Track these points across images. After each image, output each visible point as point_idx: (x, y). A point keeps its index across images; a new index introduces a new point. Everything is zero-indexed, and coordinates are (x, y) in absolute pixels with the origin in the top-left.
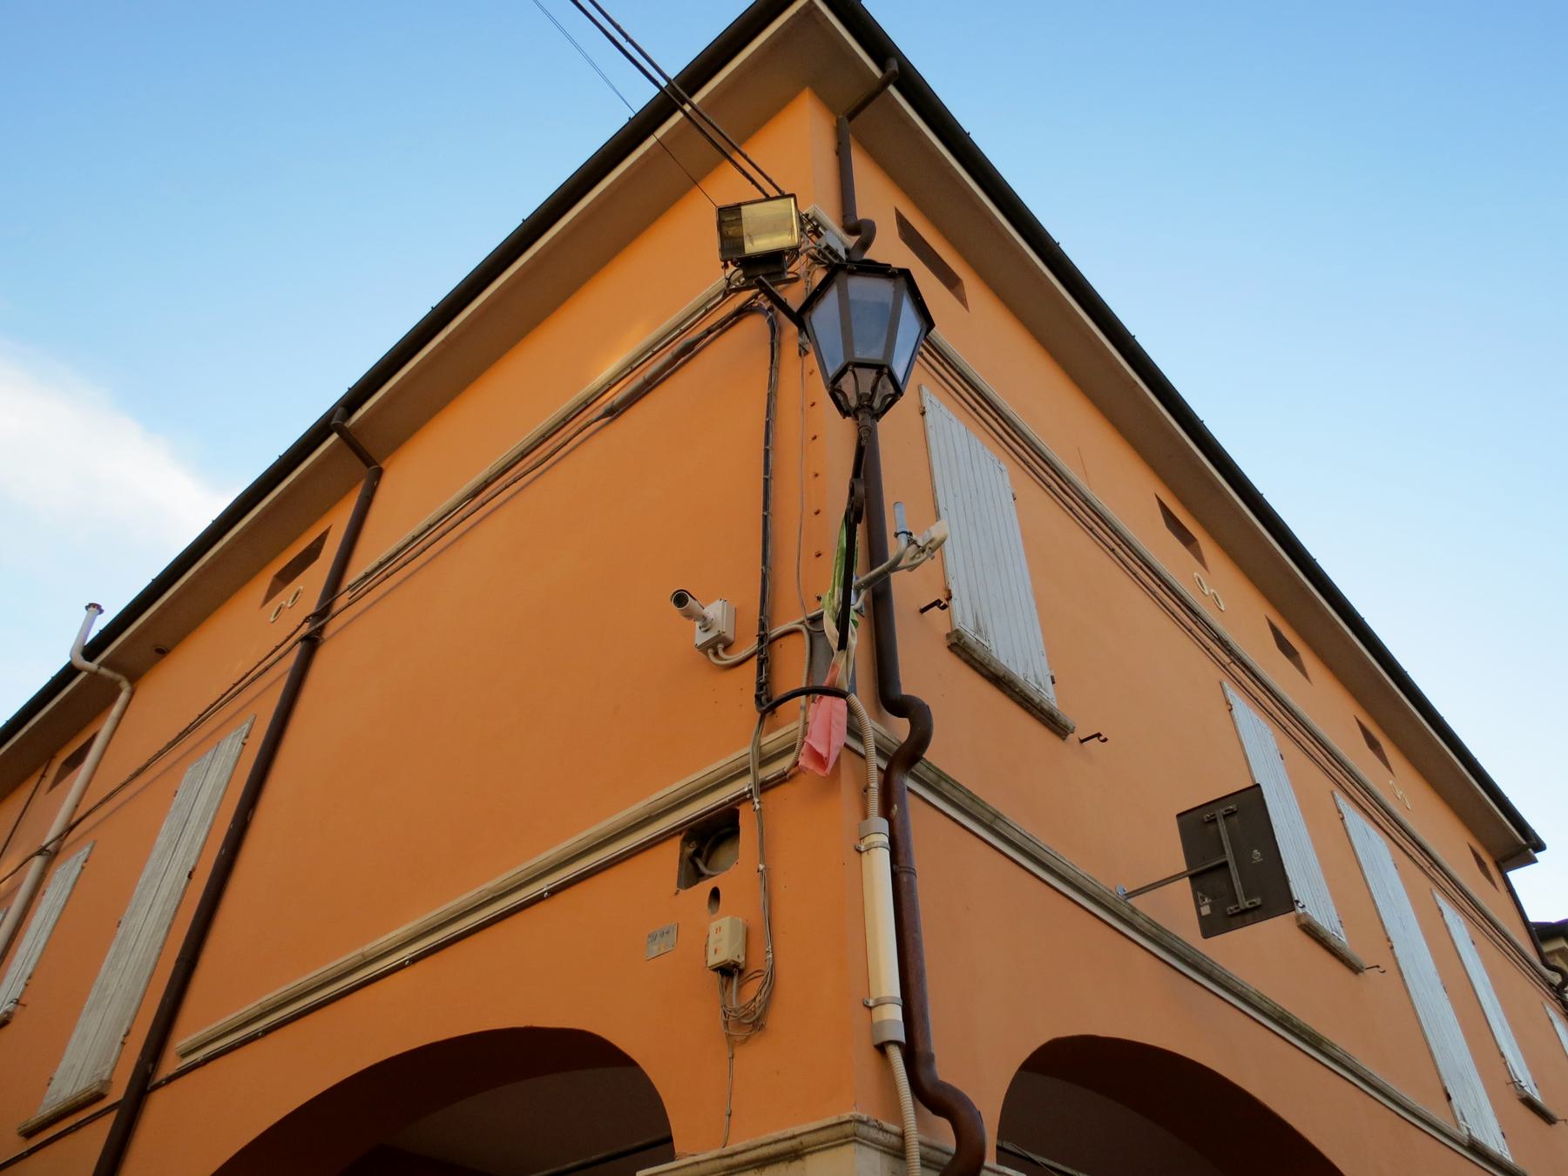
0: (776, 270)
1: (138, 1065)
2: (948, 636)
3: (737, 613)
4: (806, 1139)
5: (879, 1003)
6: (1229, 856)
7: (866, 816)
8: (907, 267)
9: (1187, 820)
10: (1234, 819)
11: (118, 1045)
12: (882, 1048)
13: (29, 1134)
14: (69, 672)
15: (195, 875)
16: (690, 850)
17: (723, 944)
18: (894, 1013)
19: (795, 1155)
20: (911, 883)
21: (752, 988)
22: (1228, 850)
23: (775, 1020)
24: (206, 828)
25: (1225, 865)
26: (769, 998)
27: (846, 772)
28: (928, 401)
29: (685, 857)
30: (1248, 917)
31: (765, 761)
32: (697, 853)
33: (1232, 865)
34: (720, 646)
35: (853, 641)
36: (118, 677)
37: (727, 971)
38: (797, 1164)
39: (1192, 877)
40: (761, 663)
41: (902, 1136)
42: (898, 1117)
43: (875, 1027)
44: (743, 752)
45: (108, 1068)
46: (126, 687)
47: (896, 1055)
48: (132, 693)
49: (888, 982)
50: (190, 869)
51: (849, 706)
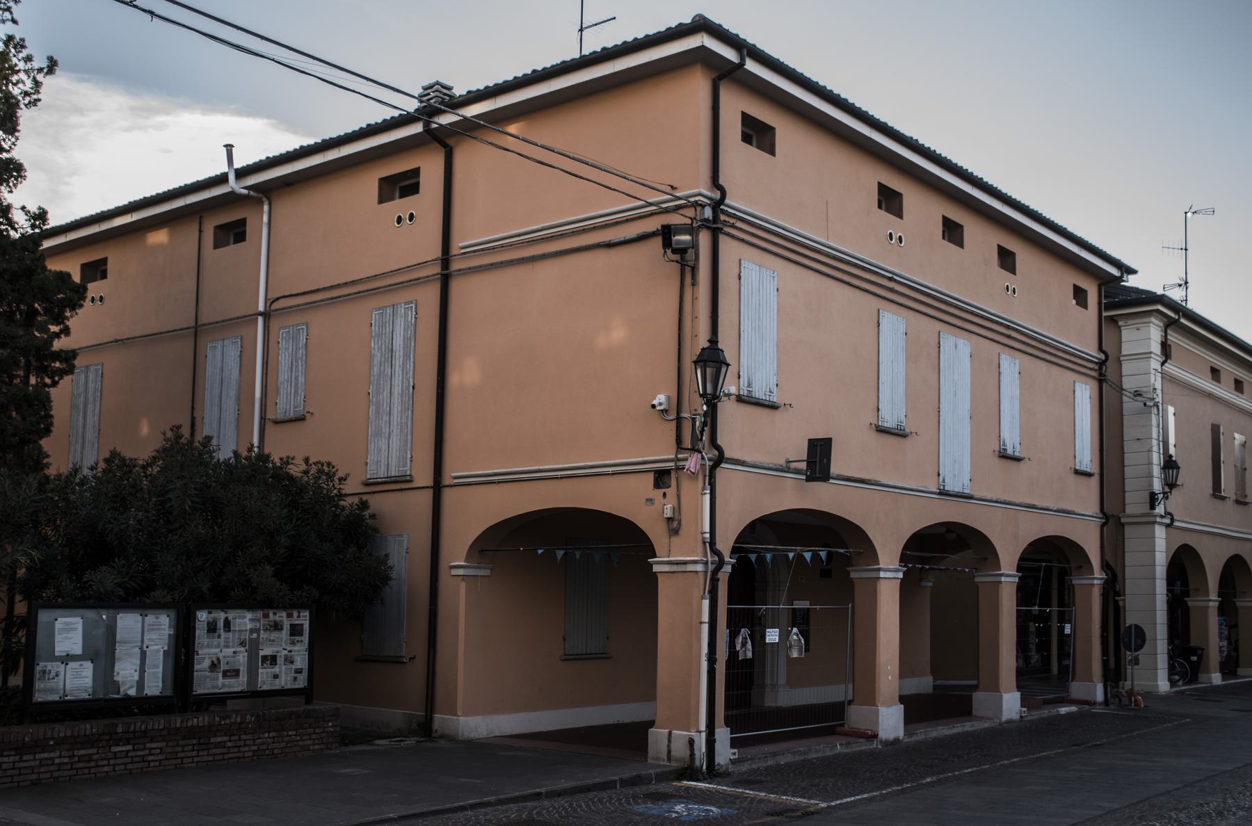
3: (669, 398)
5: (705, 533)
6: (818, 460)
8: (742, 142)
9: (809, 440)
12: (704, 543)
13: (367, 484)
16: (657, 475)
17: (668, 513)
18: (708, 535)
22: (818, 457)
23: (682, 532)
26: (680, 526)
32: (659, 477)
35: (704, 438)
36: (260, 195)
37: (669, 519)
39: (808, 462)
42: (706, 556)
43: (704, 538)
46: (264, 199)
47: (708, 545)
49: (707, 528)
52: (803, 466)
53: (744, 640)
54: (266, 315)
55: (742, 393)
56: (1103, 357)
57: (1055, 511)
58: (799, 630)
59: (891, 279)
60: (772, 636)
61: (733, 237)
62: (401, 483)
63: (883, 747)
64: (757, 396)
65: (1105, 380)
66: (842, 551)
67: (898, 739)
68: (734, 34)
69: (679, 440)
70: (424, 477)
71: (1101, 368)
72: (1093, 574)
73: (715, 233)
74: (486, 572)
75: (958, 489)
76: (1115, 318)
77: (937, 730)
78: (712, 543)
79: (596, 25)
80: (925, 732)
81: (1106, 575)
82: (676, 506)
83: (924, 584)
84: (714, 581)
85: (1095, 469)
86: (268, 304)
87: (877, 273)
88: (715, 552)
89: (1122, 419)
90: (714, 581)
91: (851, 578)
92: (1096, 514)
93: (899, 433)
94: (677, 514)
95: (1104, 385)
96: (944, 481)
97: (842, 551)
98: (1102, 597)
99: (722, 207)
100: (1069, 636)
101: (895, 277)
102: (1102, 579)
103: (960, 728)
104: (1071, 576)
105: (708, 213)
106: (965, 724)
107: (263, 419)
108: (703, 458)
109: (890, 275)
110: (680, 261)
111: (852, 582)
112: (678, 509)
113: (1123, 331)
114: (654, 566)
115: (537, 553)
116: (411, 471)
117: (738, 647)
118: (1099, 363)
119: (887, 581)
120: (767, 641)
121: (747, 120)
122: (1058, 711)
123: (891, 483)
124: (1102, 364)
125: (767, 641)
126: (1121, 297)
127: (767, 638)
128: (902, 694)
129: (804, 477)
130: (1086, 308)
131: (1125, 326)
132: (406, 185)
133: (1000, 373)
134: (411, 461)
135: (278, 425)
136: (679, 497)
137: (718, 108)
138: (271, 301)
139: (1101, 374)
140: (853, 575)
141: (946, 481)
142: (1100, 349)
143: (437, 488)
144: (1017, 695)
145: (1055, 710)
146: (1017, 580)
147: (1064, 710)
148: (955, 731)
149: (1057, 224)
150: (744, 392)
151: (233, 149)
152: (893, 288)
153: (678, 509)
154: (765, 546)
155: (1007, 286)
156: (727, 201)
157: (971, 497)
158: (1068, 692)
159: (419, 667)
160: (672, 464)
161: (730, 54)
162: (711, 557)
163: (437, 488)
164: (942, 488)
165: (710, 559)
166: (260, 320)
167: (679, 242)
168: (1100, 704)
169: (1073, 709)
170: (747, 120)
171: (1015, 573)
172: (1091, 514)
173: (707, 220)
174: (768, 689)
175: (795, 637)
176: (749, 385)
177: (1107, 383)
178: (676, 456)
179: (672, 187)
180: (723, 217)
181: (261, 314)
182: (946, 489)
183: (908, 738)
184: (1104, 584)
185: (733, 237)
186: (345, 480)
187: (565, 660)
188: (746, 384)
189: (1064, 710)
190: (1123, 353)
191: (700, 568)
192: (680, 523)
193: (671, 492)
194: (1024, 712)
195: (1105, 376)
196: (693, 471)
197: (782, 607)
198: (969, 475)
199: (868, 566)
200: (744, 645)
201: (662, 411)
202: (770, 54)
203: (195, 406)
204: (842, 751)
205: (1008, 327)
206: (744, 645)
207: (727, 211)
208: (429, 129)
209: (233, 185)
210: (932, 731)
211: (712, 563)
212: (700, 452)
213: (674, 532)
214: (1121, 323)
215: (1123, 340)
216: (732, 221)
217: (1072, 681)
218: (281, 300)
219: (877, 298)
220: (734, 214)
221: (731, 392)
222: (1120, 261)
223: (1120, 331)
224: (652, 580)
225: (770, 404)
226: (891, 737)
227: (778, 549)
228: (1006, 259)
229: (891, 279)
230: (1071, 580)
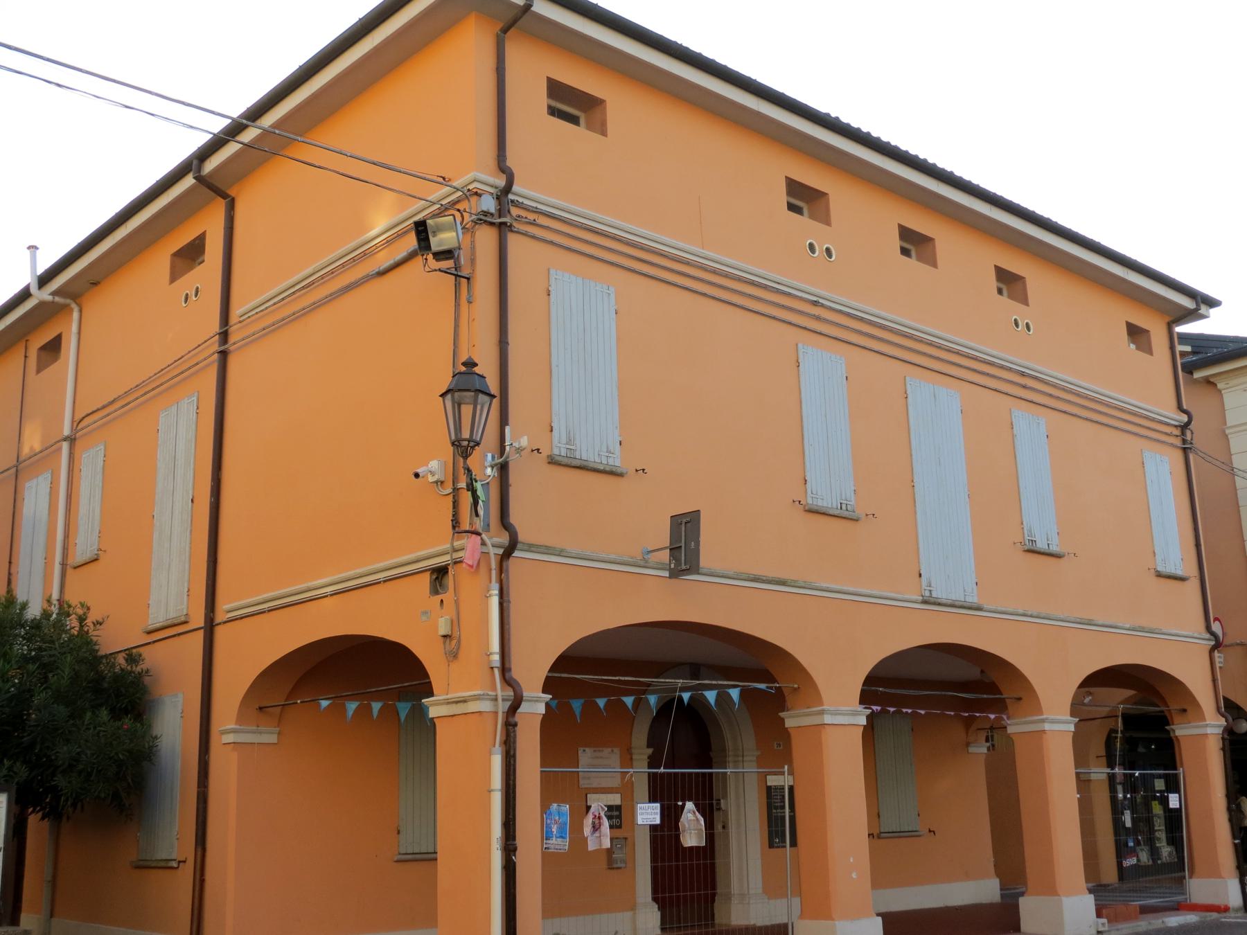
0: (449, 256)
1: (206, 615)
2: (548, 456)
4: (467, 698)
5: (491, 654)
7: (490, 582)
10: (689, 525)
11: (185, 596)
14: (25, 295)
15: (194, 500)
16: (434, 577)
17: (443, 630)
19: (465, 701)
20: (508, 607)
21: (454, 642)
23: (461, 654)
24: (192, 472)
25: (681, 547)
27: (482, 564)
28: (554, 279)
29: (432, 580)
30: (685, 572)
31: (456, 551)
32: (437, 578)
33: (683, 548)
34: (439, 483)
36: (68, 301)
38: (466, 704)
39: (670, 549)
40: (454, 496)
41: (497, 695)
42: (494, 689)
43: (490, 661)
44: (447, 546)
45: (184, 606)
46: (73, 305)
47: (497, 672)
48: (81, 311)
49: (495, 646)
50: (191, 497)
51: (482, 539)
52: (665, 556)
53: (597, 821)
54: (72, 440)
55: (556, 452)
56: (1185, 418)
58: (696, 805)
59: (815, 303)
60: (647, 813)
61: (525, 234)
62: (174, 629)
64: (584, 457)
65: (1190, 449)
66: (762, 686)
69: (456, 523)
70: (198, 620)
71: (1183, 433)
72: (1205, 720)
73: (503, 228)
74: (273, 739)
75: (957, 596)
76: (1212, 380)
78: (505, 669)
79: (1006, 394)
81: (1226, 721)
82: (455, 618)
83: (972, 750)
84: (510, 726)
85: (1191, 570)
86: (75, 424)
87: (789, 295)
88: (508, 681)
89: (1239, 512)
90: (510, 726)
91: (787, 728)
92: (1200, 634)
93: (845, 516)
94: (456, 628)
95: (1191, 457)
97: (762, 686)
98: (1222, 752)
99: (511, 197)
100: (1179, 811)
102: (1220, 726)
104: (1173, 724)
105: (489, 204)
107: (64, 565)
108: (483, 543)
109: (815, 299)
110: (453, 271)
111: (787, 731)
112: (456, 622)
113: (1225, 396)
115: (319, 705)
116: (187, 610)
117: (587, 830)
118: (1180, 426)
120: (640, 822)
121: (556, 89)
122: (1163, 922)
124: (1184, 427)
125: (640, 822)
126: (1215, 351)
129: (667, 574)
130: (1150, 352)
131: (1227, 388)
132: (192, 253)
133: (1013, 436)
134: (188, 595)
135: (77, 569)
136: (457, 602)
137: (504, 69)
138: (78, 422)
139: (1184, 441)
140: (789, 723)
142: (1180, 407)
143: (210, 627)
144: (1089, 901)
145: (1161, 921)
146: (1072, 728)
147: (1174, 920)
150: (560, 450)
151: (37, 251)
153: (456, 622)
154: (617, 678)
155: (1015, 320)
156: (515, 188)
157: (979, 609)
158: (1184, 894)
159: (186, 876)
160: (447, 557)
162: (503, 690)
163: (210, 627)
164: (927, 594)
165: (499, 693)
166: (65, 445)
167: (441, 242)
168: (1237, 910)
169: (1191, 918)
170: (556, 89)
171: (1069, 718)
172: (1190, 634)
173: (486, 213)
174: (735, 901)
175: (690, 816)
176: (569, 442)
177: (1197, 454)
178: (452, 544)
179: (444, 179)
180: (515, 211)
181: (65, 439)
182: (934, 595)
184: (1223, 734)
185: (525, 234)
186: (101, 624)
187: (397, 861)
188: (564, 440)
189: (1174, 920)
190: (1229, 424)
191: (486, 706)
192: (459, 641)
193: (448, 596)
194: (1103, 924)
195: (1191, 443)
196: (470, 563)
197: (662, 770)
198: (974, 576)
199: (808, 708)
200: (596, 828)
201: (436, 482)
203: (13, 561)
205: (1023, 374)
206: (596, 828)
207: (522, 203)
208: (200, 176)
209: (45, 295)
211: (503, 700)
212: (479, 534)
213: (454, 655)
214: (1220, 386)
215: (1227, 407)
216: (531, 217)
217: (1191, 877)
218: (85, 419)
220: (536, 208)
221: (522, 444)
223: (1222, 395)
227: (642, 682)
228: (1008, 281)
229: (815, 303)
230: (1174, 731)
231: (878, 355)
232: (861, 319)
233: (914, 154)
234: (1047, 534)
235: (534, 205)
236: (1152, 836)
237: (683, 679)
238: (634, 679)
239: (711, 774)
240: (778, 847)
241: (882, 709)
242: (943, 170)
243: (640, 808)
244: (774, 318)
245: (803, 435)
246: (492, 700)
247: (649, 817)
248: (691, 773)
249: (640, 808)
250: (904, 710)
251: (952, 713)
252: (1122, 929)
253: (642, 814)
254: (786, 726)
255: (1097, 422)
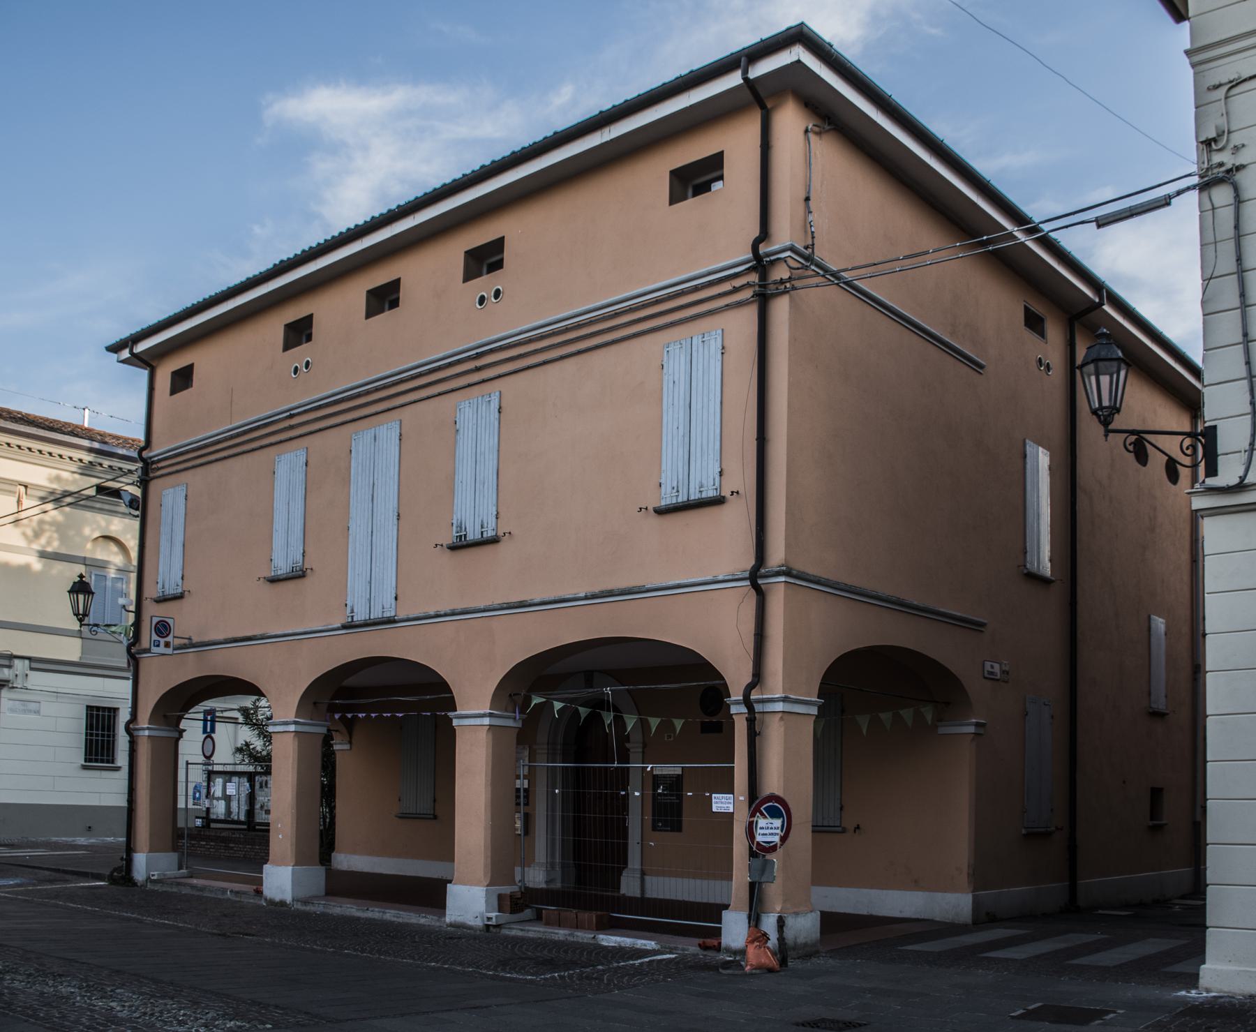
57: (586, 598)
59: (292, 416)
60: (722, 803)
63: (268, 905)
67: (286, 903)
68: (637, 97)
77: (341, 907)
80: (325, 904)
96: (352, 611)
101: (292, 412)
103: (377, 914)
106: (387, 911)
109: (288, 414)
114: (731, 706)
119: (279, 735)
123: (290, 631)
127: (227, 790)
128: (725, 883)
141: (355, 610)
148: (369, 915)
149: (254, 276)
152: (476, 367)
161: (734, 80)
183: (302, 905)
202: (712, 61)
204: (231, 898)
210: (334, 906)
219: (276, 446)
220: (477, 353)
222: (175, 314)
224: (451, 734)
225: (173, 596)
226: (278, 898)
231: (443, 397)
232: (459, 362)
233: (541, 138)
234: (482, 521)
235: (474, 352)
236: (251, 819)
237: (430, 695)
238: (436, 696)
239: (628, 768)
240: (661, 830)
241: (366, 716)
242: (268, 270)
243: (715, 798)
244: (415, 402)
245: (498, 478)
246: (513, 718)
247: (722, 805)
248: (601, 767)
249: (715, 798)
250: (385, 715)
251: (429, 714)
252: (528, 931)
253: (717, 803)
254: (453, 725)
255: (440, 394)
